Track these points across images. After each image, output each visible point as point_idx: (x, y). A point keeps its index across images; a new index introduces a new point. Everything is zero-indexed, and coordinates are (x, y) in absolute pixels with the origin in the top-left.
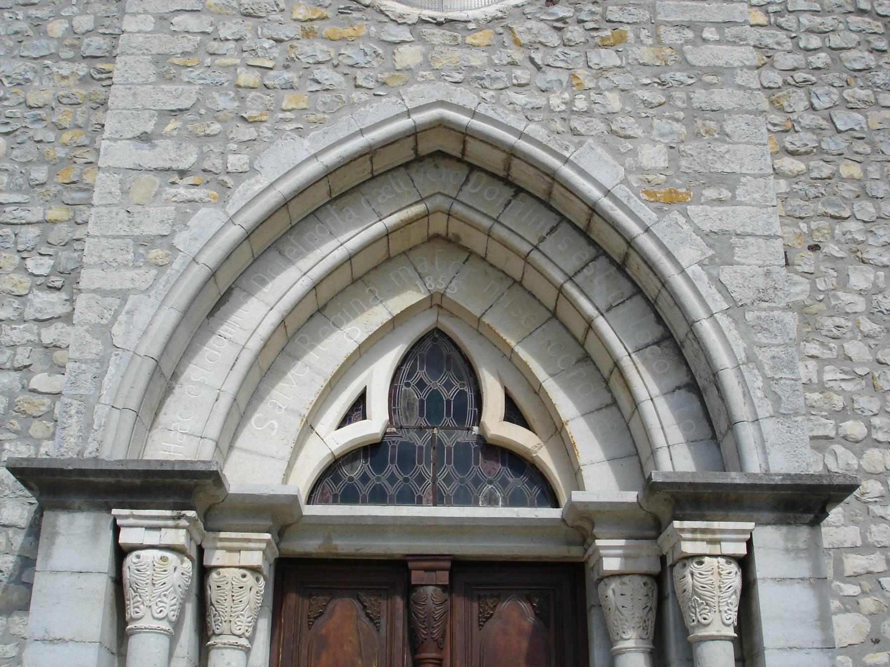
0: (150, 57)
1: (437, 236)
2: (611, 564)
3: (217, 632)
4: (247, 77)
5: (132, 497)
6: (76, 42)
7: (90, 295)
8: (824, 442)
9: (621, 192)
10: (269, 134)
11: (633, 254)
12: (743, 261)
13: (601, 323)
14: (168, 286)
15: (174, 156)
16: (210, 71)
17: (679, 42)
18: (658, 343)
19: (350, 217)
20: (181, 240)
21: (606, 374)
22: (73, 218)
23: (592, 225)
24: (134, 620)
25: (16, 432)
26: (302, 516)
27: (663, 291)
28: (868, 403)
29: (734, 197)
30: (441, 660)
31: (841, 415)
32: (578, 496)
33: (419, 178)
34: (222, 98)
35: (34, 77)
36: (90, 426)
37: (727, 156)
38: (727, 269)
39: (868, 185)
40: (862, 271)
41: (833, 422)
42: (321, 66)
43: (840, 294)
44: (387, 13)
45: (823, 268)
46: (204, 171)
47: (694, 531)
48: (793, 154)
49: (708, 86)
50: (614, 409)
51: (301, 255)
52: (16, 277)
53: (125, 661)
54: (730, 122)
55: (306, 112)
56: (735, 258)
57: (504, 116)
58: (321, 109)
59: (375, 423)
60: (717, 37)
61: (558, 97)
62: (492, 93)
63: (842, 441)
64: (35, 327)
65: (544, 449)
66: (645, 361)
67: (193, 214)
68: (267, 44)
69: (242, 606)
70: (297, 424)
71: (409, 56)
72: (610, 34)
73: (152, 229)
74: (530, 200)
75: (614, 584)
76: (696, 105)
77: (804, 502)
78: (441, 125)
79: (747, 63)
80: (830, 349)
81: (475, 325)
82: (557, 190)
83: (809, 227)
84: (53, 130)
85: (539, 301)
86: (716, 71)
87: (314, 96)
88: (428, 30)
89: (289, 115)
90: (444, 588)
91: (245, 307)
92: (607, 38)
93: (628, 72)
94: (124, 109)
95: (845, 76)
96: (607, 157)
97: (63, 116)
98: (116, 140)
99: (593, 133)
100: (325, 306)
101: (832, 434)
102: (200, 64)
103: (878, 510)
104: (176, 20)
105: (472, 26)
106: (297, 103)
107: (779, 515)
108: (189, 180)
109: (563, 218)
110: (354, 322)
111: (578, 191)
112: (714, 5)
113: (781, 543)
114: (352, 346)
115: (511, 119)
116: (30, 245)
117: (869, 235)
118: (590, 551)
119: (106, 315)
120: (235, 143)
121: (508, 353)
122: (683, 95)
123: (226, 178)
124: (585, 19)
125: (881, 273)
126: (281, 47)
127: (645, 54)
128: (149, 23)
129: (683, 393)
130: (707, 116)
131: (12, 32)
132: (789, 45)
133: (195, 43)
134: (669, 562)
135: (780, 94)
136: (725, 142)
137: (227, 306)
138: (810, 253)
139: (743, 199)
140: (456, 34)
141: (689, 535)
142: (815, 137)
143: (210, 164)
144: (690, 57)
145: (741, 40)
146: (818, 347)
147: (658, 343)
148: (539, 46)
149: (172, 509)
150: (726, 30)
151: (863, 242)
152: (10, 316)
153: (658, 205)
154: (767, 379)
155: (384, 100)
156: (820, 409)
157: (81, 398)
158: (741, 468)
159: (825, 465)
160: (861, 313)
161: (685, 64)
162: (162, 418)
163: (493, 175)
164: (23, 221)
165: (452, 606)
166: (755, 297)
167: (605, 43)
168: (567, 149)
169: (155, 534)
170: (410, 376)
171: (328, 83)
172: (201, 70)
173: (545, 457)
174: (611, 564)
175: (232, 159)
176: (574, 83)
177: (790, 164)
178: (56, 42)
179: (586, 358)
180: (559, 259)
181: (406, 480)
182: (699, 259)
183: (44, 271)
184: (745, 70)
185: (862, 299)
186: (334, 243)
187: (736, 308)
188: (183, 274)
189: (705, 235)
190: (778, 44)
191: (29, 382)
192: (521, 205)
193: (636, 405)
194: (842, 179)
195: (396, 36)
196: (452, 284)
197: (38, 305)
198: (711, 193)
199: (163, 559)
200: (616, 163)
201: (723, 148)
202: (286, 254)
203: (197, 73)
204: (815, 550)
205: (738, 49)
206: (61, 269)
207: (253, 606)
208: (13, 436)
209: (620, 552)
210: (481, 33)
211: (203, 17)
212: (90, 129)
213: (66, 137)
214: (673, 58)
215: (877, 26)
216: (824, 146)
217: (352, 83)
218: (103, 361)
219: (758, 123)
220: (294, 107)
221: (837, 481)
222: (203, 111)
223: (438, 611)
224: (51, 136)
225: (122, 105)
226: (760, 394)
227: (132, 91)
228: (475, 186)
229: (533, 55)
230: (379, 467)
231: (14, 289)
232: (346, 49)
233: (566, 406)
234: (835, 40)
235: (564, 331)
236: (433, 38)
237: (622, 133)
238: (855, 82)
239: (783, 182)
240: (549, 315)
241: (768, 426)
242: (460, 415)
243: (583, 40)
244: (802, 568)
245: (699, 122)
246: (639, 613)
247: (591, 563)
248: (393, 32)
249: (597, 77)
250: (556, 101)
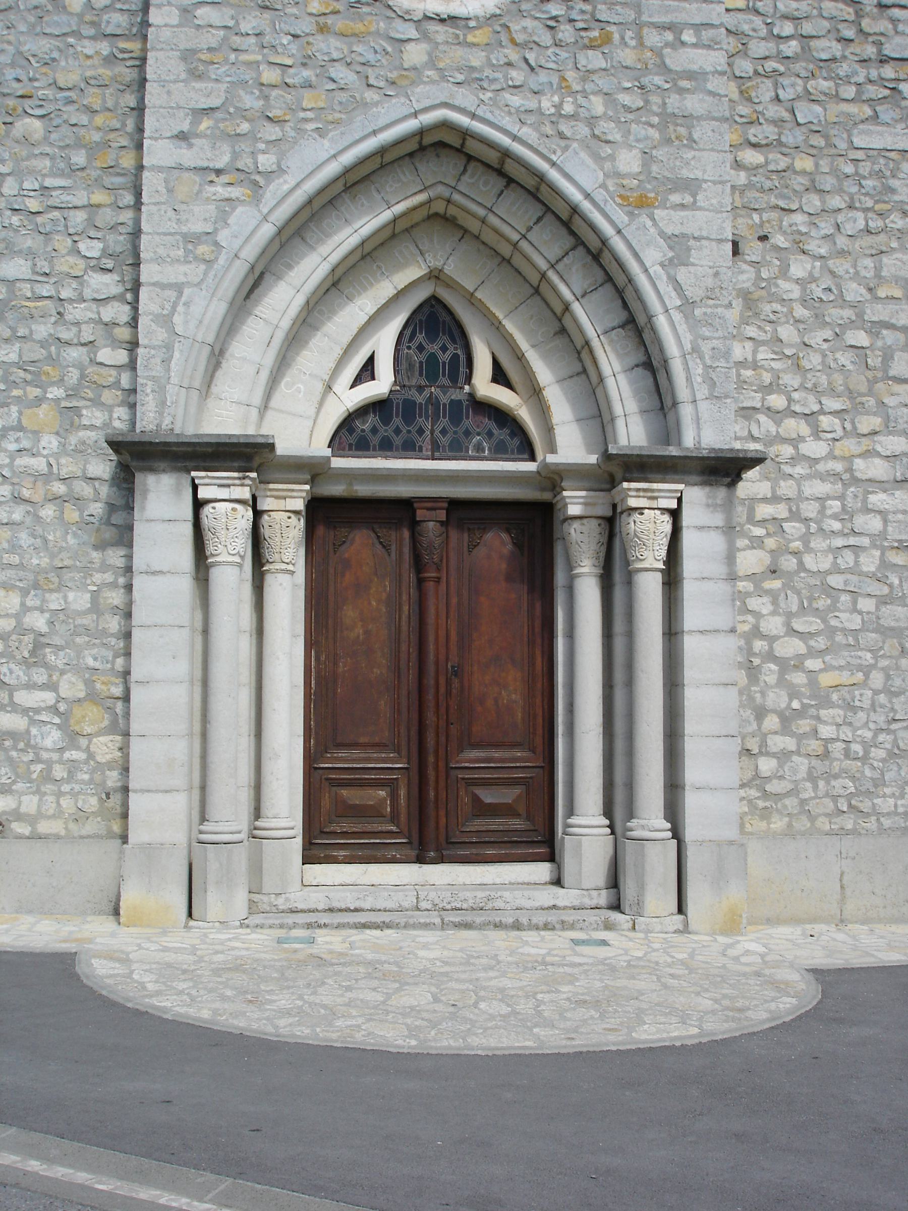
0: (178, 53)
1: (436, 215)
2: (574, 510)
3: (270, 560)
4: (270, 75)
5: (204, 461)
6: (95, 19)
7: (151, 288)
8: (751, 411)
9: (600, 196)
10: (293, 134)
11: (606, 252)
12: (696, 262)
13: (577, 308)
14: (217, 280)
15: (210, 155)
16: (234, 69)
17: (659, 45)
18: (622, 326)
19: (362, 205)
20: (223, 237)
21: (579, 348)
22: (116, 202)
23: (573, 220)
24: (213, 555)
25: (90, 400)
26: (330, 468)
27: (629, 285)
28: (791, 380)
29: (695, 202)
30: (439, 578)
31: (767, 389)
32: (551, 459)
33: (422, 168)
34: (248, 97)
35: (60, 56)
36: (163, 403)
37: (692, 163)
38: (683, 269)
39: (817, 179)
40: (801, 260)
41: (760, 395)
42: (336, 64)
43: (780, 282)
44: (394, 8)
45: (768, 258)
46: (238, 170)
47: (638, 490)
48: (755, 146)
49: (681, 91)
50: (583, 377)
51: (320, 241)
52: (71, 260)
53: (208, 585)
54: (698, 129)
55: (325, 112)
56: (691, 260)
57: (500, 118)
58: (337, 108)
59: (383, 384)
60: (694, 40)
61: (549, 100)
62: (489, 95)
63: (766, 411)
64: (94, 306)
65: (524, 408)
66: (611, 342)
67: (232, 213)
68: (286, 40)
69: (289, 540)
70: (320, 387)
71: (415, 54)
72: (597, 35)
73: (198, 227)
74: (519, 189)
75: (576, 525)
76: (669, 110)
77: (724, 470)
78: (445, 125)
79: (719, 68)
80: (766, 332)
81: (468, 297)
82: (544, 188)
83: (761, 218)
84: (85, 113)
85: (524, 278)
86: (690, 75)
87: (331, 95)
88: (433, 27)
89: (310, 115)
90: (442, 523)
91: (276, 290)
92: (595, 39)
93: (612, 74)
94: (161, 107)
95: (811, 67)
96: (589, 161)
97: (93, 98)
98: (156, 139)
99: (578, 137)
100: (339, 280)
101: (759, 405)
102: (226, 60)
103: (787, 469)
104: (199, 12)
105: (472, 24)
106: (316, 103)
107: (705, 478)
108: (225, 178)
109: (548, 209)
110: (364, 295)
111: (563, 193)
112: (695, 5)
113: (704, 500)
114: (363, 318)
115: (507, 122)
116: (80, 229)
117: (812, 226)
118: (558, 498)
119: (167, 306)
120: (263, 142)
121: (497, 324)
122: (659, 101)
123: (258, 178)
124: (576, 18)
125: (818, 264)
126: (298, 42)
127: (627, 56)
128: (174, 17)
129: (640, 371)
130: (679, 121)
131: (31, 7)
132: (764, 32)
133: (219, 39)
134: (619, 510)
135: (750, 84)
136: (692, 148)
137: (261, 288)
138: (759, 243)
139: (703, 204)
140: (458, 32)
141: (634, 493)
142: (776, 130)
143: (243, 163)
144: (668, 61)
145: (716, 44)
146: (756, 329)
147: (622, 326)
148: (533, 45)
149: (239, 471)
150: (704, 33)
151: (806, 233)
152: (70, 296)
153: (630, 208)
154: (707, 367)
155: (394, 101)
156: (751, 384)
157: (153, 379)
158: (679, 444)
159: (750, 431)
160: (795, 300)
161: (663, 68)
162: (214, 389)
163: (488, 166)
164: (70, 206)
165: (447, 537)
166: (703, 295)
167: (593, 44)
168: (554, 153)
169: (224, 490)
170: (411, 339)
171: (342, 82)
172: (227, 67)
173: (525, 415)
174: (574, 510)
175: (261, 158)
176: (563, 85)
177: (751, 157)
178: (76, 19)
179: (563, 331)
180: (543, 248)
181: (409, 432)
182: (660, 260)
183: (96, 253)
184: (716, 75)
185: (798, 287)
186: (348, 230)
187: (688, 305)
188: (227, 269)
189: (669, 238)
190: (754, 30)
191: (96, 356)
192: (511, 195)
193: (601, 379)
194: (796, 172)
195: (403, 34)
196: (450, 261)
197: (95, 286)
198: (675, 198)
199: (234, 509)
200: (597, 168)
201: (689, 155)
202: (308, 241)
203: (224, 69)
204: (728, 506)
205: (712, 53)
206: (111, 252)
207: (297, 540)
208: (89, 403)
209: (582, 500)
210: (480, 31)
211: (224, 9)
212: (120, 112)
213: (99, 120)
214: (652, 61)
215: (849, 13)
216: (783, 139)
217: (364, 82)
218: (168, 347)
219: (722, 130)
220: (314, 106)
221: (749, 455)
222: (232, 110)
223: (437, 542)
224: (84, 119)
225: (158, 103)
226: (699, 379)
227: (166, 89)
228: (472, 176)
229: (527, 57)
230: (386, 421)
231: (71, 271)
232: (358, 46)
233: (544, 374)
234: (807, 28)
235: (545, 306)
236: (437, 36)
237: (603, 138)
238: (821, 72)
239: (743, 174)
240: (532, 291)
241: (703, 406)
242: (454, 377)
243: (573, 40)
244: (718, 519)
245: (671, 128)
246: (594, 547)
247: (559, 506)
248: (400, 29)
249: (584, 80)
250: (547, 104)
